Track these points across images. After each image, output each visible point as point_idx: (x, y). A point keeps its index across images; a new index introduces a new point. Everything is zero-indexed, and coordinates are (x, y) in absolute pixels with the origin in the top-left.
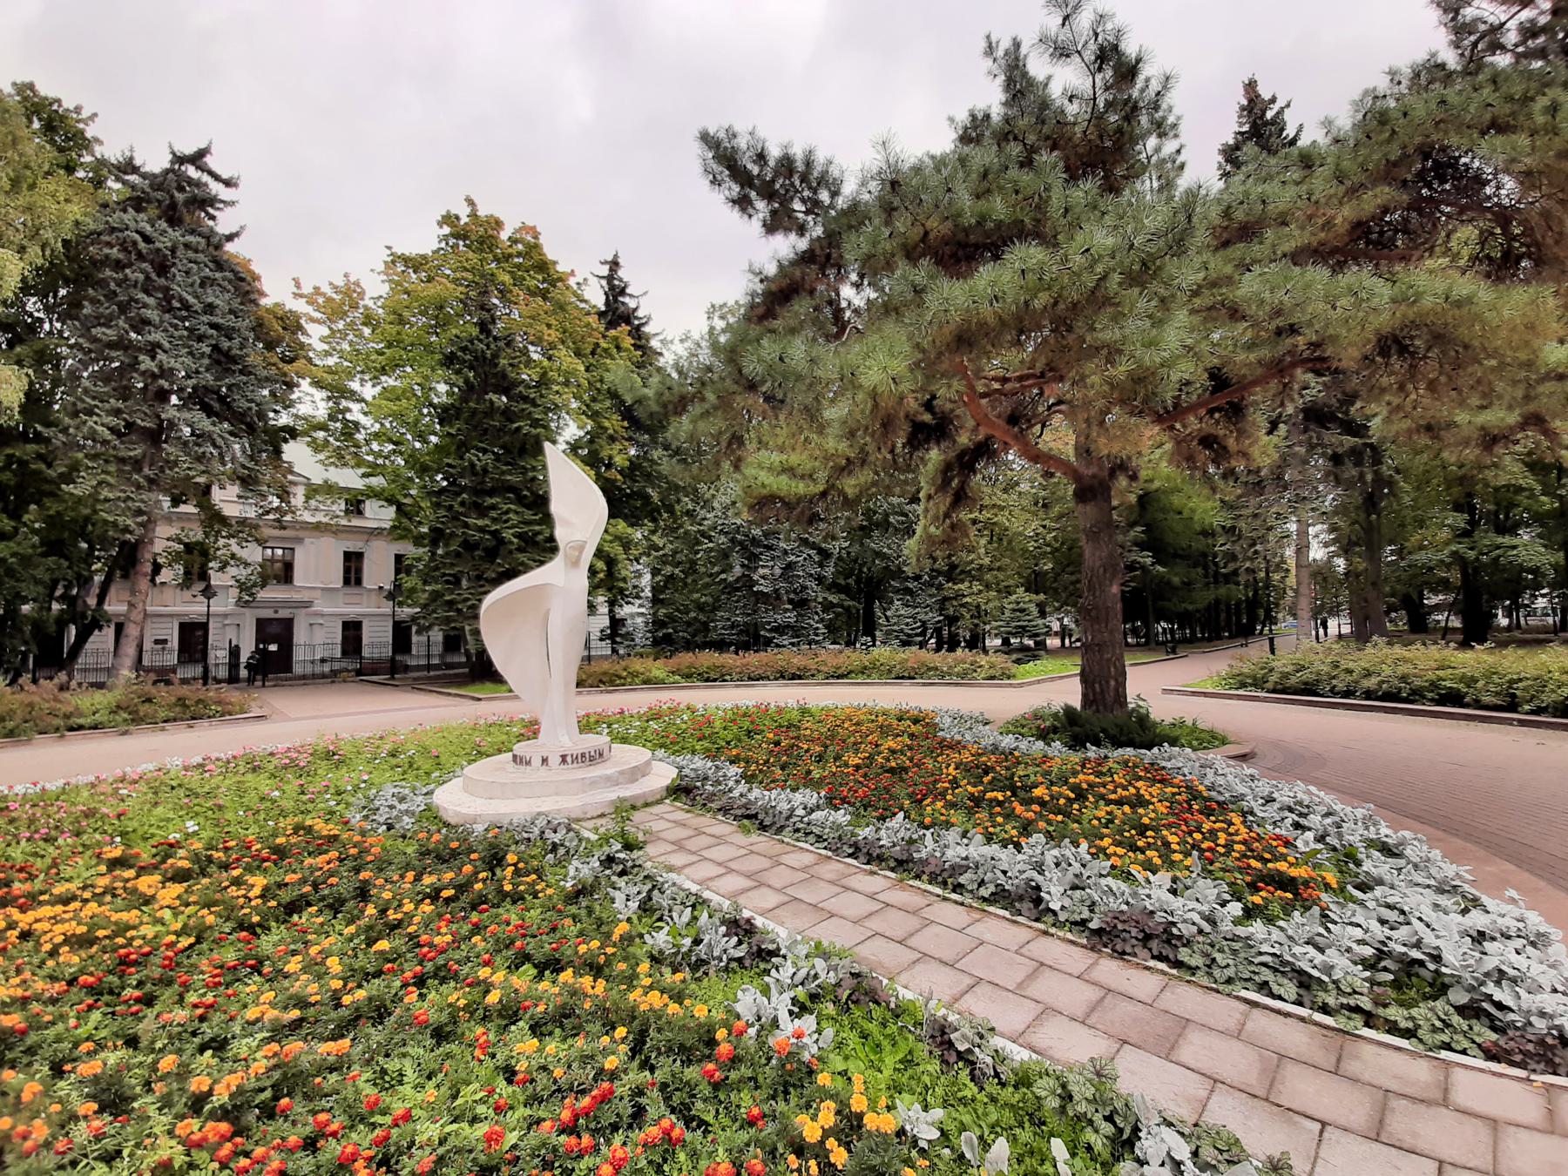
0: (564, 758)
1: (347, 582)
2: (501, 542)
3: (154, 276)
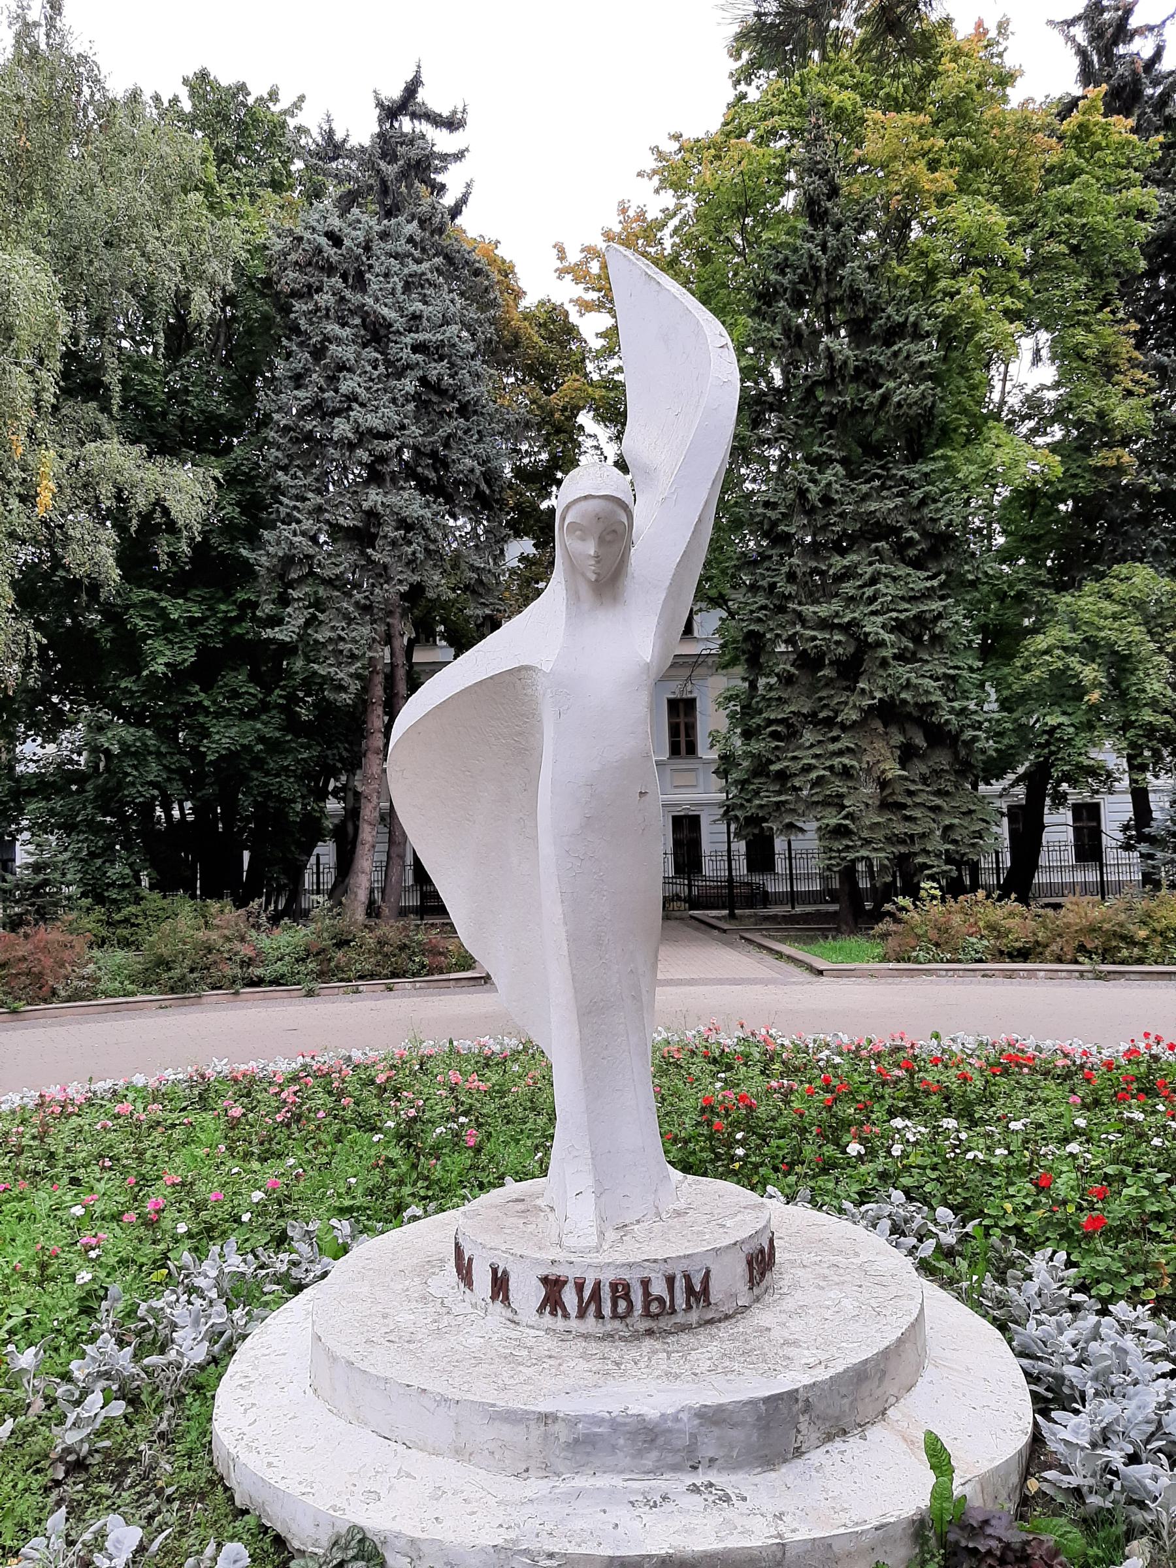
0: (553, 1286)
1: (675, 751)
2: (865, 646)
3: (348, 293)
